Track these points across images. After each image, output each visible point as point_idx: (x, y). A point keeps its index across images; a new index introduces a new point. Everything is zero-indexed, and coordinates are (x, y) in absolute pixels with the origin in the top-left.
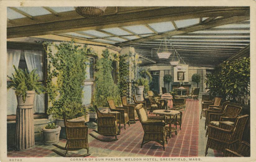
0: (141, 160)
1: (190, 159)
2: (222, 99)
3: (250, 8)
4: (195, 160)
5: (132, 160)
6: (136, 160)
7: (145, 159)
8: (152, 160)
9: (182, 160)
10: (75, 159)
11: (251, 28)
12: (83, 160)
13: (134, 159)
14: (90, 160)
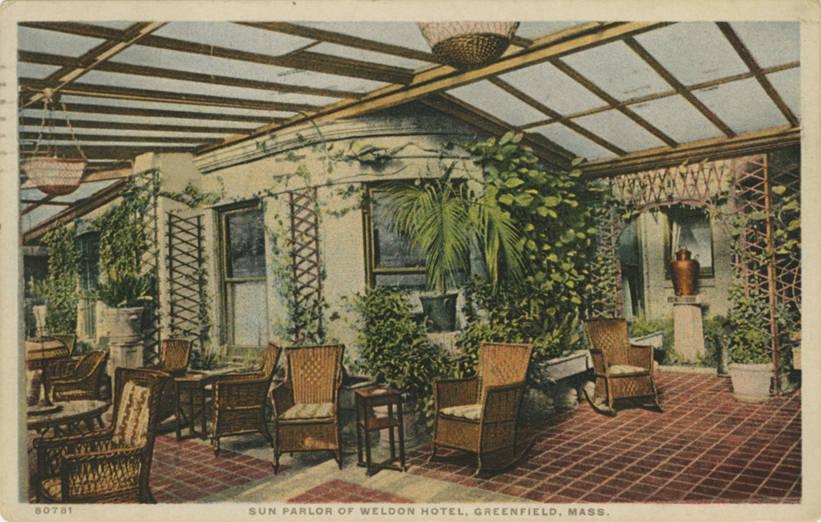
0: (274, 513)
1: (570, 510)
2: (106, 286)
3: (796, 506)
4: (587, 512)
5: (544, 514)
6: (396, 513)
7: (427, 511)
8: (447, 512)
9: (311, 513)
10: (404, 510)
11: (12, 58)
12: (454, 514)
13: (390, 509)
14: (403, 513)
